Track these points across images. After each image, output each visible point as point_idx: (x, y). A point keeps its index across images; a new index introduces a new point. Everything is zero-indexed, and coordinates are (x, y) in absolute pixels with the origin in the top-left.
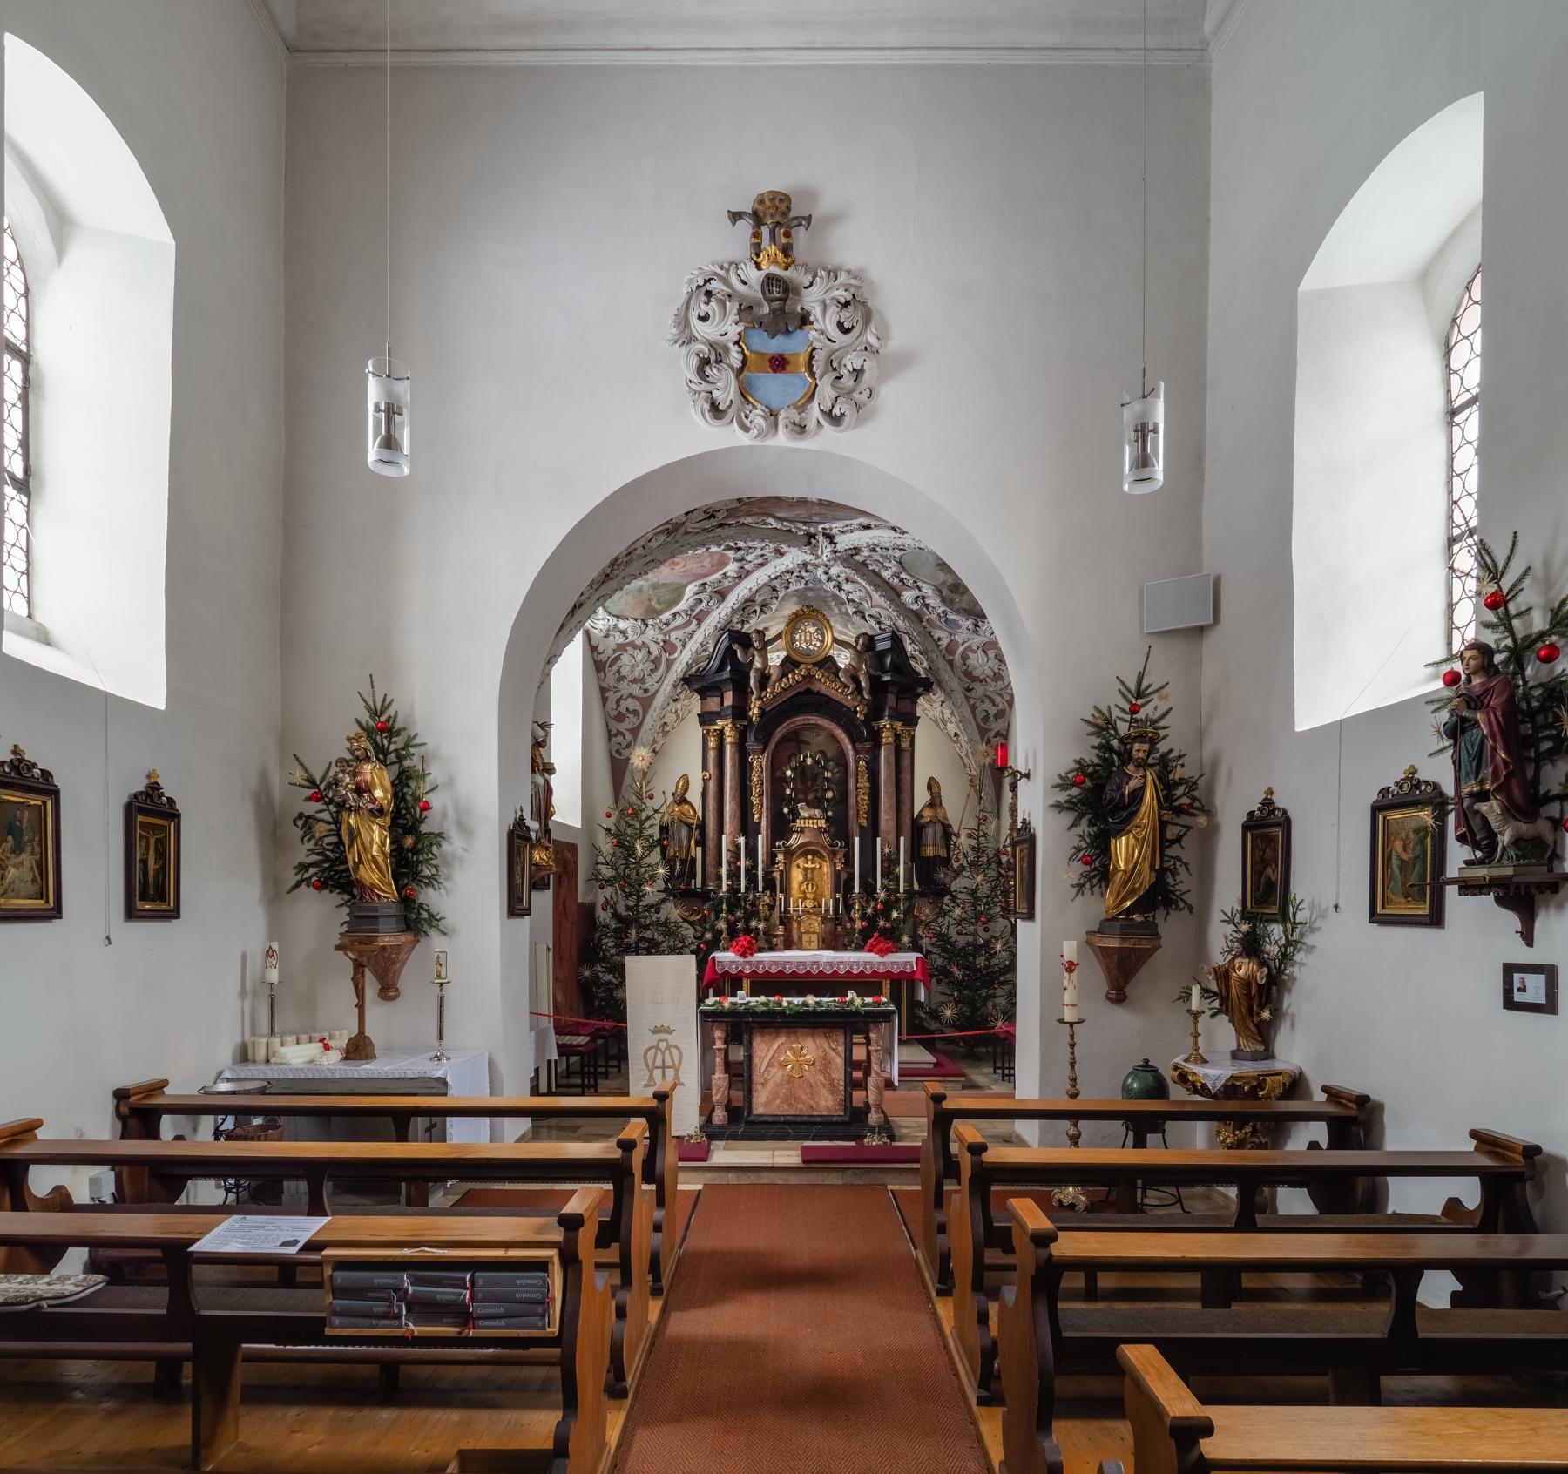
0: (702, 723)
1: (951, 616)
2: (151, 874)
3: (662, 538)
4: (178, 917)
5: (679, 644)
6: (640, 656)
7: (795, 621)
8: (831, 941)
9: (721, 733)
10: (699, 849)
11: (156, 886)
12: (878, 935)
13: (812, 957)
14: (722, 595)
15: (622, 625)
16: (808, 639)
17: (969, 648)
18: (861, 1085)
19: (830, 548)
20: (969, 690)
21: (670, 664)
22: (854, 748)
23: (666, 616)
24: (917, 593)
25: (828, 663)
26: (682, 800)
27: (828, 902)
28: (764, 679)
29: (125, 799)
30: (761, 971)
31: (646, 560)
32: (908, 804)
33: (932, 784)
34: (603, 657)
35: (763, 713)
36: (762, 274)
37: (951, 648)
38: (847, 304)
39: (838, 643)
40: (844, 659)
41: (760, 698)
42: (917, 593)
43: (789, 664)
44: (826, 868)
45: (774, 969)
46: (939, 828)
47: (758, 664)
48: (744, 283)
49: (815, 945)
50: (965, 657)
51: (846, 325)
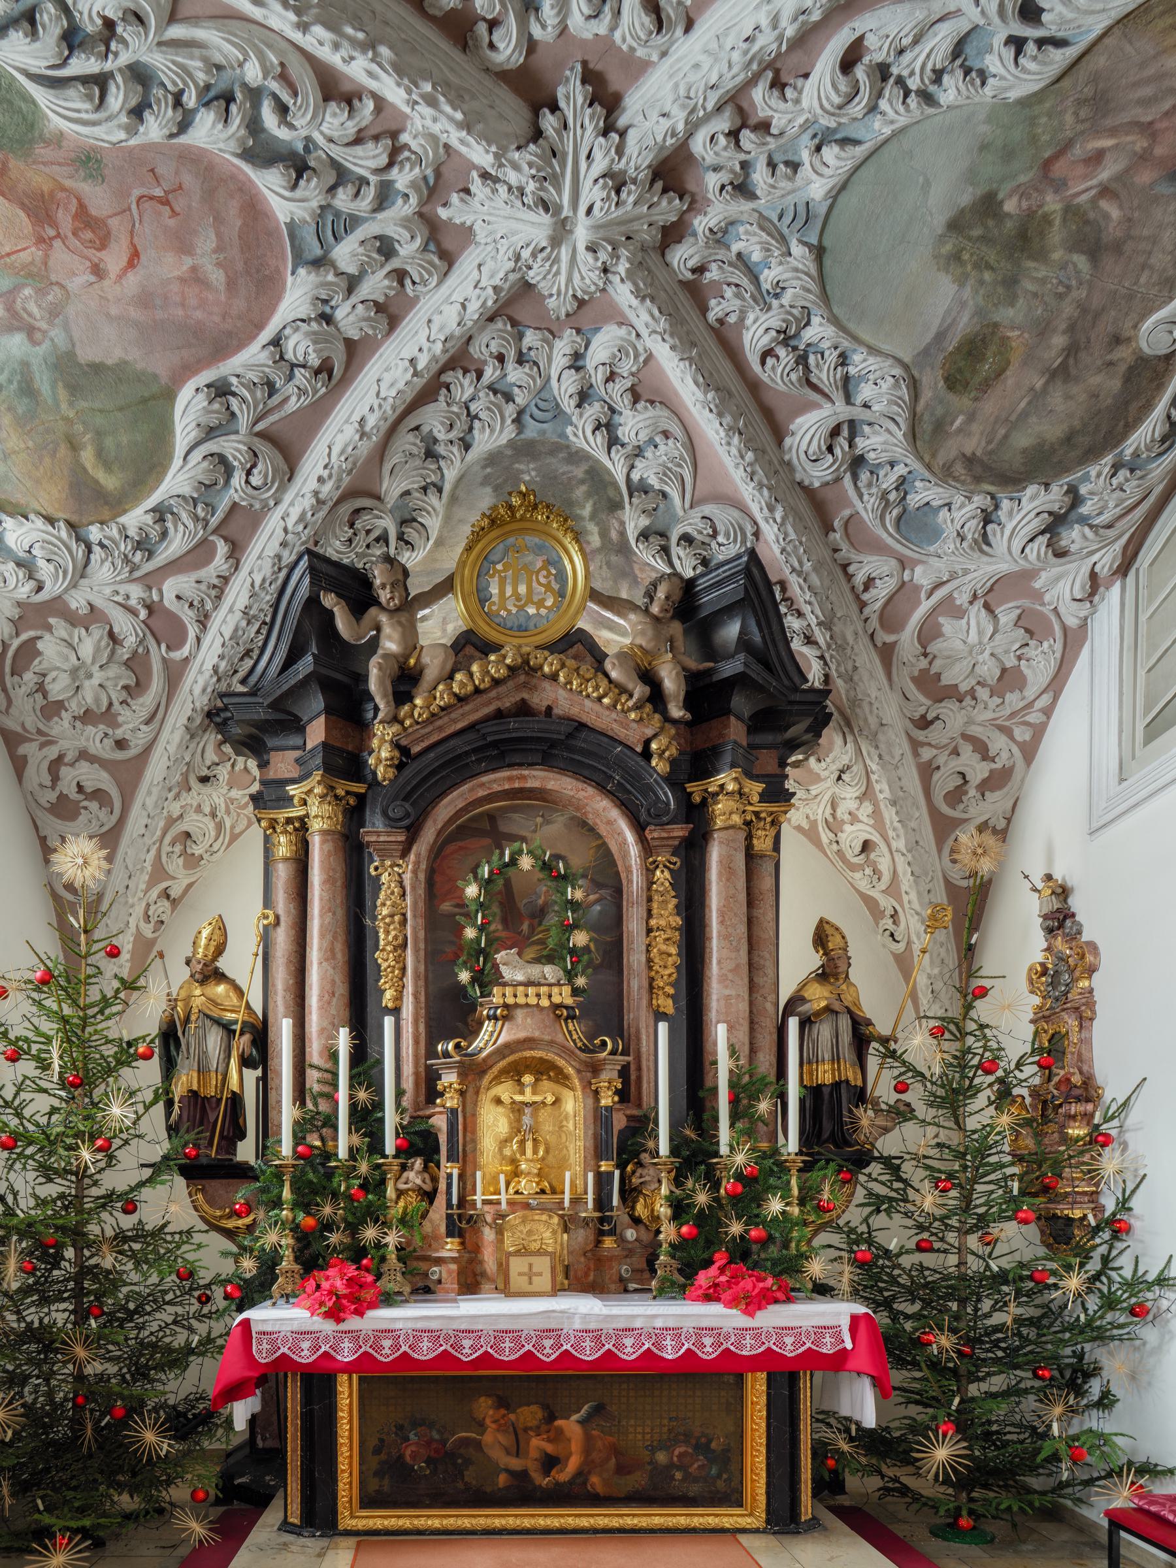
5: (188, 616)
6: (89, 644)
8: (584, 1275)
9: (301, 827)
12: (725, 1248)
13: (530, 1312)
14: (284, 448)
16: (521, 597)
21: (174, 675)
22: (642, 839)
23: (136, 518)
25: (576, 645)
26: (210, 974)
27: (577, 1177)
30: (386, 1354)
33: (821, 938)
39: (599, 608)
40: (617, 634)
43: (470, 645)
44: (573, 1103)
45: (425, 1352)
46: (845, 1023)
47: (391, 644)
49: (544, 1282)
50: (928, 634)
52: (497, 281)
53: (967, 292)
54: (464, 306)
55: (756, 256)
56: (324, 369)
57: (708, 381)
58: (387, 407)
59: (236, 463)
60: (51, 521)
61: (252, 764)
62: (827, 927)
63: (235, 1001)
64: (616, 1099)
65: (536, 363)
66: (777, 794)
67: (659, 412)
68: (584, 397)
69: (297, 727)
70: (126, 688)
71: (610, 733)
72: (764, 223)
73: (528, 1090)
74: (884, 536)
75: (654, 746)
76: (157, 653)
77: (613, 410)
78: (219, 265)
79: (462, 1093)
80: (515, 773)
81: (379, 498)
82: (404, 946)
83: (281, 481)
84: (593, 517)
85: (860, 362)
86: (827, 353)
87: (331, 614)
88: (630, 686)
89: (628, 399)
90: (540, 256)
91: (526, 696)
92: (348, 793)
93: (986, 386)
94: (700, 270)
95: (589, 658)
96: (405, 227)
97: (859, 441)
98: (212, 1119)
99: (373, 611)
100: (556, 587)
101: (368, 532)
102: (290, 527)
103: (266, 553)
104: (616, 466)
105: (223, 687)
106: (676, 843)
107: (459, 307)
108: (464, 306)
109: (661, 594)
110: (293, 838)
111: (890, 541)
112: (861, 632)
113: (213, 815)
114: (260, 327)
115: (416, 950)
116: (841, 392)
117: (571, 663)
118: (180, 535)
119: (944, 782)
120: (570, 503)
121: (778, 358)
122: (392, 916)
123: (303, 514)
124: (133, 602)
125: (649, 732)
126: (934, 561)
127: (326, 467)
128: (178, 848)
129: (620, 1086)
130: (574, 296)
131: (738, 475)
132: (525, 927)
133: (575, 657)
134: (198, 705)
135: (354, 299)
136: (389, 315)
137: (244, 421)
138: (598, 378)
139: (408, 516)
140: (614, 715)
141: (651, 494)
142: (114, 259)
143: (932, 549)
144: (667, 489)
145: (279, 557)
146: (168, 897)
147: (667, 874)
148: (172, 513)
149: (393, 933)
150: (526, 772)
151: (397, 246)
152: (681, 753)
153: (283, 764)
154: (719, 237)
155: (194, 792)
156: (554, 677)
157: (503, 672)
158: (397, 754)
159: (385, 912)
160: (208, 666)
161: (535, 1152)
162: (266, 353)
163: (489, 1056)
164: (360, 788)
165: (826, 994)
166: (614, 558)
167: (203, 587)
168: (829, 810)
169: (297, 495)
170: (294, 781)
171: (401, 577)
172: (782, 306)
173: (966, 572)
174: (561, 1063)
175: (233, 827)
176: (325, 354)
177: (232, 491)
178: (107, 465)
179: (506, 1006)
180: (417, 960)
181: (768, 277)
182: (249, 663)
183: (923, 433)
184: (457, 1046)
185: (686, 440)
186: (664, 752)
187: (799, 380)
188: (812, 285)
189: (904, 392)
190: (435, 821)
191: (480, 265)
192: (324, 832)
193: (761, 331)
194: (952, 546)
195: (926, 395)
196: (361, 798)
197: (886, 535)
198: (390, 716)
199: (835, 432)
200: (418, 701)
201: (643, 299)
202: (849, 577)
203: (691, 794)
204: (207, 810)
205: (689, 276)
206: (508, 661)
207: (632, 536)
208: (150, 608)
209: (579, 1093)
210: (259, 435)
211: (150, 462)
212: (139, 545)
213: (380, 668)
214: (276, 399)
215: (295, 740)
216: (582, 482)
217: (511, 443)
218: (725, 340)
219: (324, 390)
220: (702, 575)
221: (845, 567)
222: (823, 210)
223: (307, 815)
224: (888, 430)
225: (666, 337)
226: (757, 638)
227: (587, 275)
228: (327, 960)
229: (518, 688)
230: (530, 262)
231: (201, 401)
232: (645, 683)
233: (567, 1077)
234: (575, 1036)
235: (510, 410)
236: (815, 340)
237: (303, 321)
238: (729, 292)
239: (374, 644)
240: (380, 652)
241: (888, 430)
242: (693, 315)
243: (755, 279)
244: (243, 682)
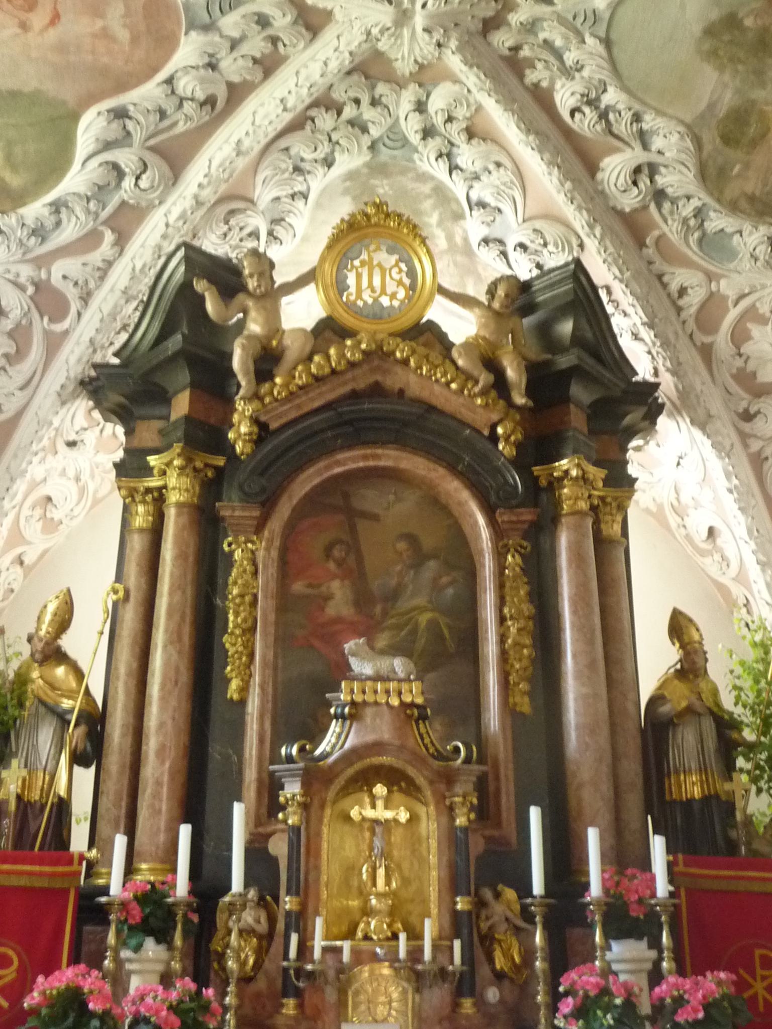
7: (353, 234)
9: (159, 497)
14: (174, 158)
16: (376, 283)
22: (492, 522)
23: (36, 210)
25: (428, 335)
28: (267, 361)
33: (679, 627)
35: (263, 431)
37: (712, 307)
41: (256, 396)
43: (329, 330)
44: (430, 827)
46: (708, 725)
47: (255, 327)
50: (739, 336)
52: (353, 47)
53: (727, 77)
54: (325, 64)
55: (559, 43)
56: (210, 101)
57: (529, 128)
58: (261, 133)
59: (127, 170)
61: (120, 430)
62: (680, 618)
63: (74, 684)
64: (472, 816)
65: (386, 107)
66: (621, 481)
67: (490, 146)
68: (428, 133)
69: (163, 398)
70: (6, 356)
71: (459, 416)
72: (561, 20)
73: (380, 804)
74: (690, 253)
75: (500, 430)
76: (40, 325)
77: (452, 144)
78: (125, 26)
79: (305, 807)
80: (369, 451)
81: (252, 201)
82: (253, 629)
83: (166, 186)
84: (440, 224)
85: (650, 121)
86: (623, 113)
87: (202, 299)
88: (476, 373)
89: (464, 136)
90: (386, 35)
91: (379, 378)
92: (207, 465)
93: (754, 143)
94: (516, 49)
95: (438, 347)
96: (279, 8)
97: (658, 178)
98: (33, 830)
99: (241, 297)
100: (407, 281)
101: (241, 229)
102: (171, 222)
103: (82, 339)
104: (458, 187)
105: (98, 359)
106: (526, 526)
107: (322, 64)
108: (325, 64)
109: (501, 292)
110: (151, 508)
111: (696, 258)
112: (680, 332)
113: (78, 479)
114: (156, 70)
115: (265, 634)
116: (638, 142)
117: (421, 350)
118: (72, 224)
120: (419, 213)
121: (584, 114)
122: (242, 596)
123: (184, 213)
124: (22, 280)
125: (495, 417)
126: (734, 276)
127: (206, 176)
128: (38, 512)
129: (475, 801)
130: (416, 61)
131: (561, 199)
132: (378, 609)
133: (425, 345)
134: (72, 375)
135: (235, 54)
136: (268, 66)
137: (138, 136)
138: (439, 121)
139: (277, 217)
140: (461, 400)
141: (488, 209)
142: (38, 19)
143: (731, 266)
144: (501, 206)
145: (159, 247)
146: (22, 563)
147: (518, 558)
148: (67, 207)
149: (243, 615)
150: (379, 451)
151: (271, 20)
152: (526, 436)
153: (148, 433)
154: (531, 27)
155: (60, 456)
156: (405, 362)
157: (358, 356)
158: (256, 429)
159: (235, 591)
160: (86, 339)
161: (388, 883)
162: (160, 89)
163: (336, 762)
164: (220, 461)
165: (687, 692)
166: (459, 258)
167: (89, 269)
168: (673, 495)
169: (180, 196)
170: (156, 451)
171: (267, 267)
172: (582, 78)
173: (764, 287)
174: (411, 771)
175: (96, 491)
176: (210, 92)
177: (122, 192)
178: (14, 168)
179: (353, 704)
180: (265, 646)
181: (570, 58)
182: (124, 336)
183: (711, 175)
184: (302, 750)
185: (515, 169)
186: (509, 436)
187: (603, 130)
188: (605, 65)
189: (689, 143)
190: (290, 498)
191: (338, 37)
192: (179, 505)
193: (568, 94)
194: (748, 265)
195: (708, 148)
196: (219, 470)
197: (692, 252)
198: (251, 393)
199: (637, 170)
200: (278, 380)
201: (471, 67)
202: (665, 286)
203: (537, 478)
204: (71, 473)
205: (507, 52)
206: (363, 346)
207: (474, 240)
208: (37, 285)
209: (432, 808)
210: (152, 149)
211: (56, 164)
212: (34, 232)
213: (244, 348)
214: (166, 123)
215: (159, 411)
216: (429, 196)
217: (367, 165)
218: (542, 98)
219: (207, 118)
220: (538, 277)
221: (660, 277)
222: (607, 16)
223: (165, 487)
224: (680, 171)
225: (492, 93)
226: (589, 335)
227: (425, 47)
228: (171, 643)
229: (373, 370)
230: (379, 36)
231: (102, 122)
232: (490, 371)
233: (418, 789)
234: (427, 740)
235: (366, 141)
236: (612, 103)
237: (193, 67)
238: (540, 66)
239: (241, 325)
240: (246, 333)
241: (680, 171)
242: (513, 81)
243: (559, 57)
244: (116, 354)
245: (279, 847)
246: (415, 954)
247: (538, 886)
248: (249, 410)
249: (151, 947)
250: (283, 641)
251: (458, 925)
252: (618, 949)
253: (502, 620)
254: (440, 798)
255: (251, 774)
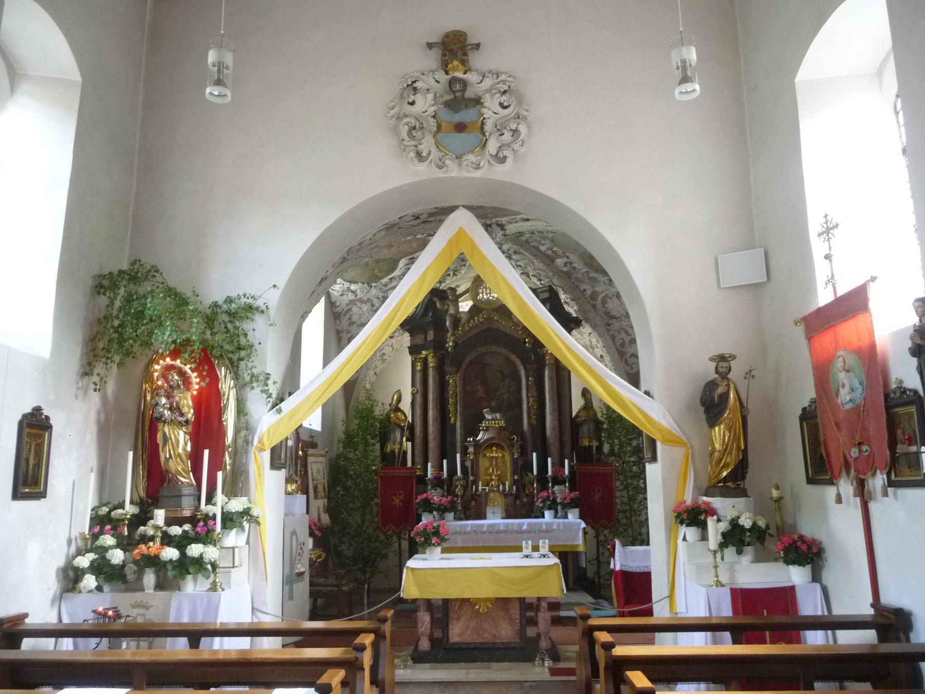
0: (411, 353)
1: (592, 275)
2: (31, 467)
3: (383, 233)
4: (45, 497)
9: (425, 361)
10: (410, 444)
11: (33, 476)
15: (353, 287)
17: (607, 296)
18: (533, 622)
19: (501, 233)
20: (608, 325)
22: (525, 368)
24: (565, 260)
28: (456, 320)
29: (19, 418)
31: (371, 247)
32: (567, 408)
34: (339, 310)
36: (449, 77)
37: (594, 296)
38: (505, 92)
41: (453, 335)
42: (565, 260)
43: (475, 310)
44: (508, 458)
46: (592, 425)
47: (452, 311)
48: (438, 82)
50: (604, 302)
51: (505, 104)
60: (363, 283)
119: (619, 342)
164: (443, 352)
239: (447, 310)
245: (468, 464)
246: (504, 490)
247: (535, 473)
248: (452, 338)
249: (439, 490)
250: (465, 406)
251: (515, 482)
252: (556, 488)
253: (528, 398)
254: (510, 450)
255: (459, 444)
